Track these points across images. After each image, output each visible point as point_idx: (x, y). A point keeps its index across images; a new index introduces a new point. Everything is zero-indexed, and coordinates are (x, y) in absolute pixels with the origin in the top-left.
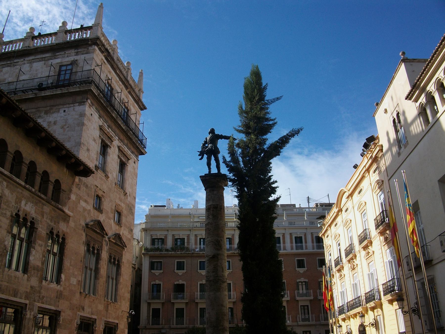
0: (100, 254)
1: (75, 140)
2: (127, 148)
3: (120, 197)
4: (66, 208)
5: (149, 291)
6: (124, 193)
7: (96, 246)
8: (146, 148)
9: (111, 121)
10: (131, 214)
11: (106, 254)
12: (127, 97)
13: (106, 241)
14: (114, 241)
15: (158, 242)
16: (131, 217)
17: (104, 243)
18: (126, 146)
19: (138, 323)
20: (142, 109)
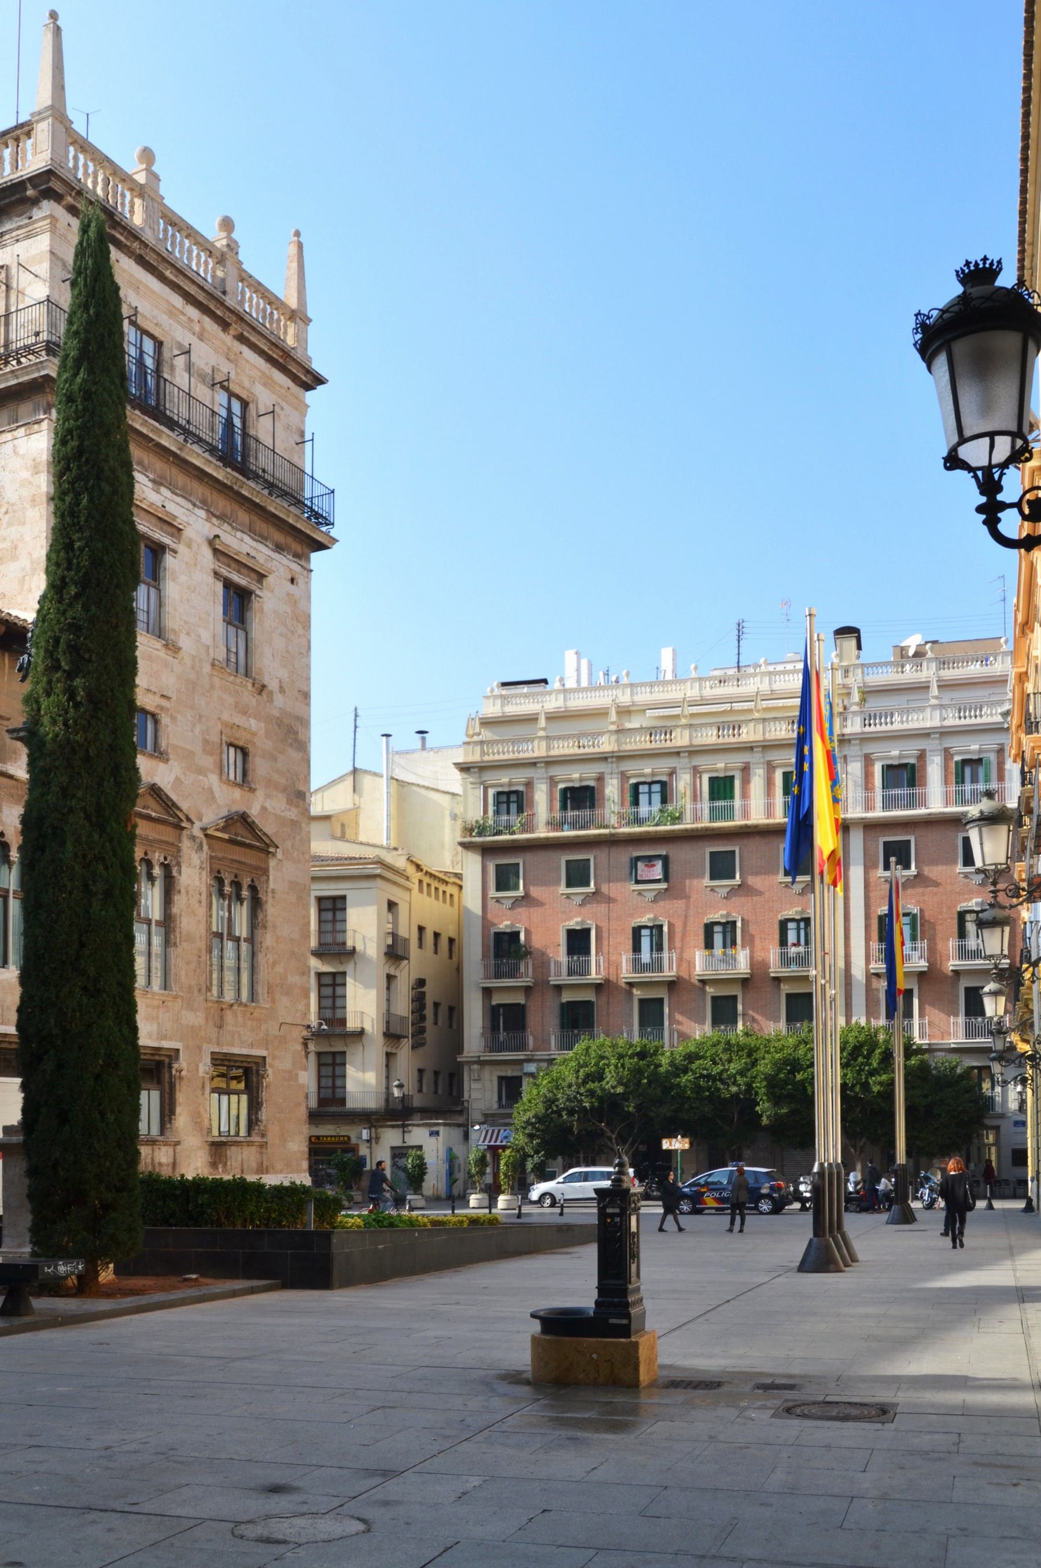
0: (174, 877)
1: (29, 553)
2: (252, 538)
3: (236, 703)
4: (18, 764)
5: (485, 956)
6: (253, 685)
7: (157, 857)
8: (333, 524)
9: (165, 460)
10: (291, 745)
11: (200, 874)
12: (232, 357)
13: (193, 838)
14: (226, 836)
15: (650, 793)
16: (295, 755)
17: (186, 845)
18: (243, 532)
19: (459, 1047)
20: (308, 387)
